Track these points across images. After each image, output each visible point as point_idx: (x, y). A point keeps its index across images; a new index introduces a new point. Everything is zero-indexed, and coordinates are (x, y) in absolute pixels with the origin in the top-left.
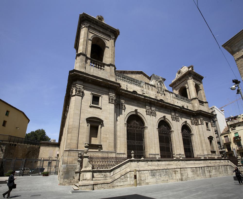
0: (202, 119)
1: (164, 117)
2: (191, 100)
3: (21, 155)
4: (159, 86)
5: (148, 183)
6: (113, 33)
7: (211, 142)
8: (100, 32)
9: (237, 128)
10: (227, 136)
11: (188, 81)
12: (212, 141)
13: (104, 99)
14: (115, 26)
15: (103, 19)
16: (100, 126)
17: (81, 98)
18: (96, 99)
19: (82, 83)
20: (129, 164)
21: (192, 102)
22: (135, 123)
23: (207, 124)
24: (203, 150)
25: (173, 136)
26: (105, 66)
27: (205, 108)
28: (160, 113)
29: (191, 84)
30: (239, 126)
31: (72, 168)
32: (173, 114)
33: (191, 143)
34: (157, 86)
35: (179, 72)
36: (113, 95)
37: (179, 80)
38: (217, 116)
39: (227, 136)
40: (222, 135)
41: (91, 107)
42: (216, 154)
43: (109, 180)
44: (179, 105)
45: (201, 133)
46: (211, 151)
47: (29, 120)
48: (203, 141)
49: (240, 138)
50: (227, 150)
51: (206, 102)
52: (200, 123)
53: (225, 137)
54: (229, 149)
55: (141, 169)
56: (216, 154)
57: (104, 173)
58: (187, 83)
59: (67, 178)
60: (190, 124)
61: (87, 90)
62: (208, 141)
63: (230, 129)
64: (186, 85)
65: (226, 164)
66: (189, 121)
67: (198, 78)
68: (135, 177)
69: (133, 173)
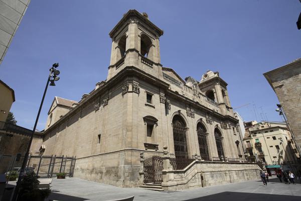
0: (230, 123)
1: (179, 111)
2: (219, 105)
3: (14, 149)
4: (195, 89)
5: (210, 184)
6: (158, 33)
7: (237, 146)
8: (147, 29)
9: (258, 135)
10: (249, 141)
11: (216, 86)
12: (153, 126)
13: (156, 98)
14: (161, 28)
15: (147, 16)
16: (155, 125)
17: (137, 95)
18: (149, 97)
19: (137, 80)
20: (195, 165)
21: (220, 106)
22: (178, 123)
23: (233, 128)
24: (232, 154)
25: (189, 134)
26: (154, 65)
27: (230, 114)
28: (197, 115)
29: (218, 88)
30: (259, 133)
31: (136, 169)
32: (207, 117)
33: (222, 146)
34: (193, 89)
35: (206, 76)
36: (163, 94)
37: (207, 83)
38: (239, 122)
39: (249, 141)
40: (244, 140)
41: (146, 105)
42: (158, 151)
43: (185, 181)
44: (211, 109)
45: (230, 137)
46: (145, 144)
47: (14, 100)
48: (232, 145)
49: (261, 144)
50: (249, 155)
51: (231, 108)
52: (228, 127)
53: (247, 142)
54: (251, 154)
55: (205, 171)
56: (158, 151)
57: (180, 174)
58: (214, 88)
59: (133, 180)
60: (205, 122)
61: (142, 87)
62: (235, 145)
63: (252, 135)
64: (214, 90)
65: (256, 168)
66: (204, 119)
67: (224, 85)
68: (202, 178)
69: (200, 174)
